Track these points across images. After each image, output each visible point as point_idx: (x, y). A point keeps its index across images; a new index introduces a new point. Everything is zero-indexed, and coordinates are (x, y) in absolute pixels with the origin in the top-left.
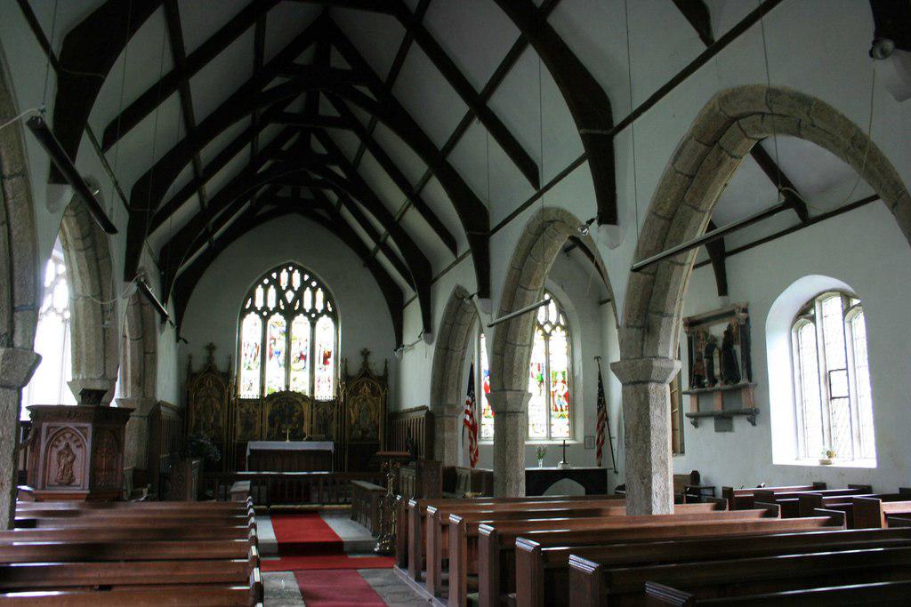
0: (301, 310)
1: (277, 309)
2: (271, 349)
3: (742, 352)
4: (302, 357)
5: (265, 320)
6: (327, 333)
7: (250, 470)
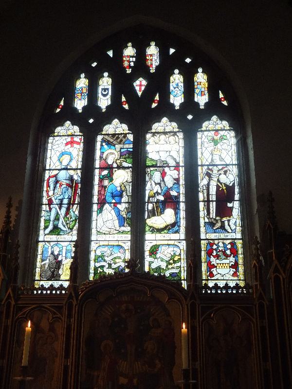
0: (166, 109)
1: (115, 111)
2: (102, 187)
3: (43, 184)
4: (170, 201)
5: (190, 133)
6: (220, 149)
7: (193, 380)
